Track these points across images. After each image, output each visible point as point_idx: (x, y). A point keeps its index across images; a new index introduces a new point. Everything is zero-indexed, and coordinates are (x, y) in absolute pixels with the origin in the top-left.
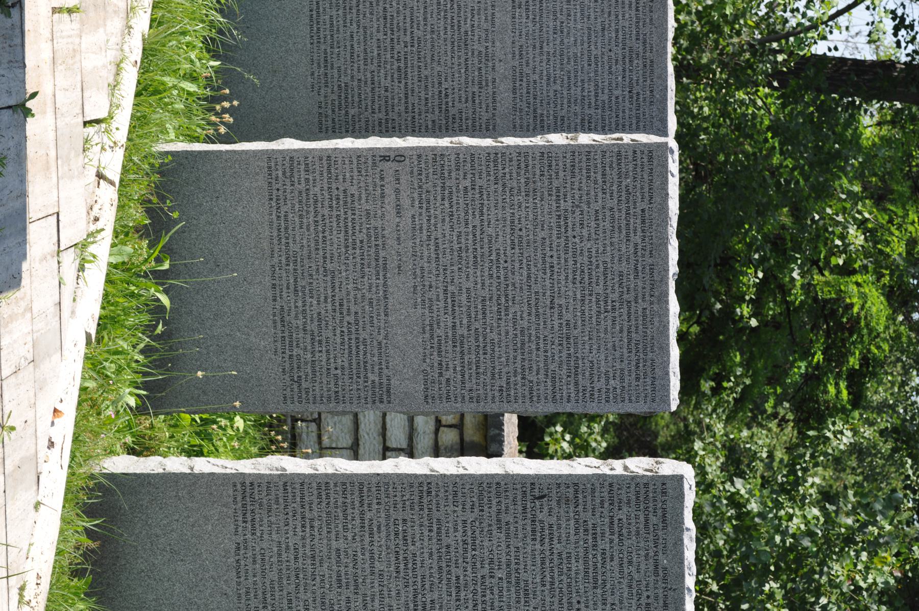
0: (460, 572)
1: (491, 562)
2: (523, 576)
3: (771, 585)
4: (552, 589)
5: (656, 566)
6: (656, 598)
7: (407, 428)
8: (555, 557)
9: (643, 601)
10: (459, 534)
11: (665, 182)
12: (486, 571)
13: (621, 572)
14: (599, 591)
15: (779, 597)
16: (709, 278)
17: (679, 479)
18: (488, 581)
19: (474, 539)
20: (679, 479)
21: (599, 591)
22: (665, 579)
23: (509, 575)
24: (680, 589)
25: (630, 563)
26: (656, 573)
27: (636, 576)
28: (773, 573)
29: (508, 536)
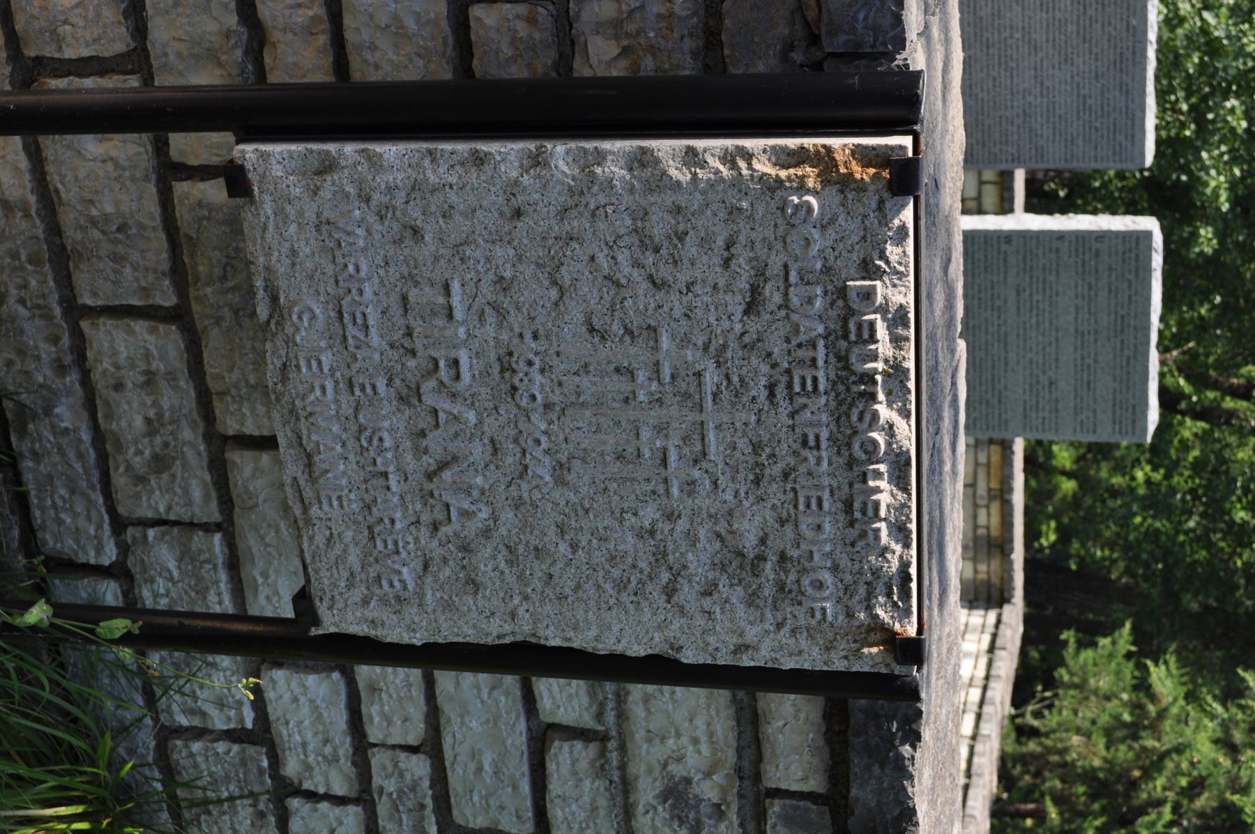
0: (989, 35)
1: (1011, 27)
2: (1034, 36)
3: (1232, 103)
4: (1054, 46)
5: (1128, 25)
6: (1128, 48)
7: (113, 490)
8: (1057, 23)
9: (1118, 50)
10: (989, 9)
11: (1145, 50)
12: (1007, 34)
13: (1103, 31)
14: (1087, 45)
15: (1239, 112)
16: (255, 45)
17: (1148, 235)
18: (1009, 41)
19: (999, 11)
20: (1148, 235)
21: (1087, 45)
22: (1134, 36)
23: (1024, 36)
24: (1144, 41)
25: (1110, 24)
26: (1128, 31)
27: (1113, 33)
28: (1236, 92)
29: (1023, 9)
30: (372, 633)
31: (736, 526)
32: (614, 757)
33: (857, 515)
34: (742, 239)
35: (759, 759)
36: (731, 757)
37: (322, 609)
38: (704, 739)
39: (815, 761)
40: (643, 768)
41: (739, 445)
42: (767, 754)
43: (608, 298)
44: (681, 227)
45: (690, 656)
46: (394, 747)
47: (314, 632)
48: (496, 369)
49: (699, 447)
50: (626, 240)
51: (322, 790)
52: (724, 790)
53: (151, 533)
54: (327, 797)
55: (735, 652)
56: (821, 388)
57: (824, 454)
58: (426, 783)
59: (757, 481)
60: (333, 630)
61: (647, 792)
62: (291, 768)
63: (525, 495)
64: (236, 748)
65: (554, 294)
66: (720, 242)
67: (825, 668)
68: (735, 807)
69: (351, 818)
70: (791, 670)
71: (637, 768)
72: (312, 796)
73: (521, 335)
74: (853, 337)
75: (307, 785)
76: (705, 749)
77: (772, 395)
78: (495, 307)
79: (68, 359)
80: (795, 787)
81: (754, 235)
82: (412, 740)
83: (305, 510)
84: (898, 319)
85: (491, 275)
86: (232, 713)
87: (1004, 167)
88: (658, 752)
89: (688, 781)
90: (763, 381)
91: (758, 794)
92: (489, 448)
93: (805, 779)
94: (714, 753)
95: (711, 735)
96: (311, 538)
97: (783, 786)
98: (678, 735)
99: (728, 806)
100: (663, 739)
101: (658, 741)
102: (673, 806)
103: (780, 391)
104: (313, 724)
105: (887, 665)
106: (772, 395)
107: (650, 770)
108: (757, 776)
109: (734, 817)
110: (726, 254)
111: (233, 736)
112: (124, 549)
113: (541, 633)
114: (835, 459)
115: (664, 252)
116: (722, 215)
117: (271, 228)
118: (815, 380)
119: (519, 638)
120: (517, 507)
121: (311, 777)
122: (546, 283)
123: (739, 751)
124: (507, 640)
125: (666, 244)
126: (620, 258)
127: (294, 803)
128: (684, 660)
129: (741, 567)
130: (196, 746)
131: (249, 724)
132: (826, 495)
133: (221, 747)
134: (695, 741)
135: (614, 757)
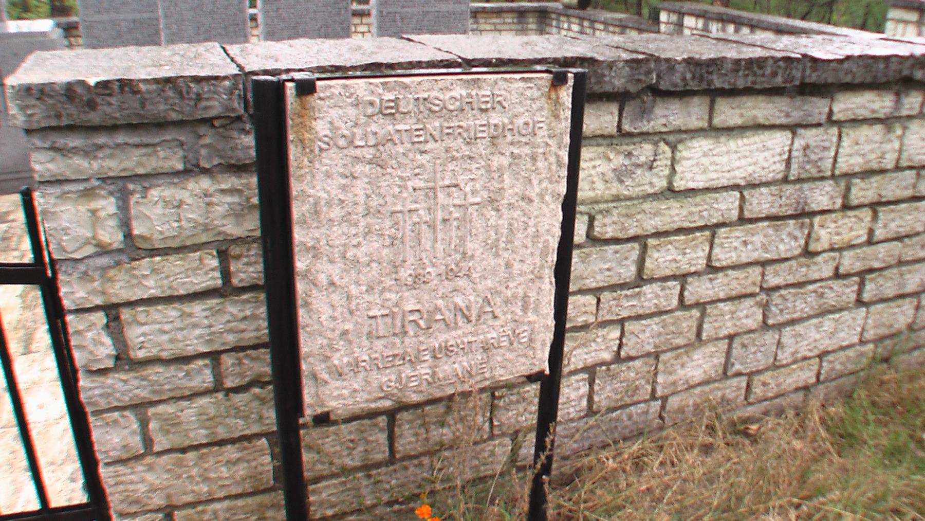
30: (549, 345)
31: (495, 168)
32: (603, 206)
33: (489, 106)
34: (341, 170)
35: (602, 136)
36: (601, 149)
37: (536, 369)
38: (593, 163)
39: (603, 108)
40: (607, 192)
41: (453, 168)
42: (599, 132)
43: (375, 238)
44: (336, 202)
45: (563, 189)
46: (597, 310)
47: (547, 372)
48: (414, 292)
49: (454, 189)
50: (345, 230)
51: (618, 342)
52: (618, 153)
53: (496, 423)
54: (621, 339)
55: (561, 167)
56: (421, 127)
57: (457, 124)
58: (615, 294)
59: (471, 158)
60: (547, 364)
61: (616, 188)
62: (607, 356)
63: (479, 275)
64: (597, 381)
65: (374, 265)
66: (344, 181)
67: (569, 121)
68: (625, 147)
69: (631, 328)
70: (571, 137)
71: (608, 194)
72: (620, 346)
73: (396, 280)
74: (393, 111)
75: (615, 349)
76: (598, 162)
77: (425, 152)
78: (382, 292)
79: (416, 462)
80: (617, 119)
81: (340, 165)
82: (594, 302)
83: (486, 379)
84: (258, 297)
85: (365, 296)
86: (581, 384)
87: (350, 14)
88: (600, 186)
89: (614, 170)
90: (418, 157)
91: (619, 136)
92: (455, 293)
93: (612, 113)
94: (600, 158)
95: (591, 160)
96: (501, 376)
97: (616, 124)
98: (591, 176)
99: (625, 151)
100: (593, 183)
101: (594, 186)
102: (626, 177)
103: (422, 147)
104: (586, 347)
105: (568, 89)
106: (425, 152)
107: (609, 189)
108: (611, 136)
109: (632, 147)
110: (351, 178)
111: (591, 383)
112: (503, 435)
113: (550, 264)
114: (459, 118)
115: (350, 210)
116: (329, 181)
117: (345, 402)
118: (417, 130)
119: (553, 275)
120: (485, 278)
121: (611, 346)
122: (368, 269)
123: (598, 145)
124: (553, 280)
125: (346, 209)
126: (354, 232)
127: (623, 354)
128: (565, 192)
129: (517, 164)
130: (596, 398)
131: (586, 376)
132: (478, 122)
133: (596, 388)
134: (594, 167)
135: (603, 206)
